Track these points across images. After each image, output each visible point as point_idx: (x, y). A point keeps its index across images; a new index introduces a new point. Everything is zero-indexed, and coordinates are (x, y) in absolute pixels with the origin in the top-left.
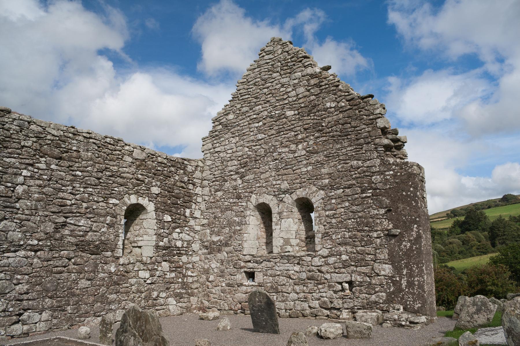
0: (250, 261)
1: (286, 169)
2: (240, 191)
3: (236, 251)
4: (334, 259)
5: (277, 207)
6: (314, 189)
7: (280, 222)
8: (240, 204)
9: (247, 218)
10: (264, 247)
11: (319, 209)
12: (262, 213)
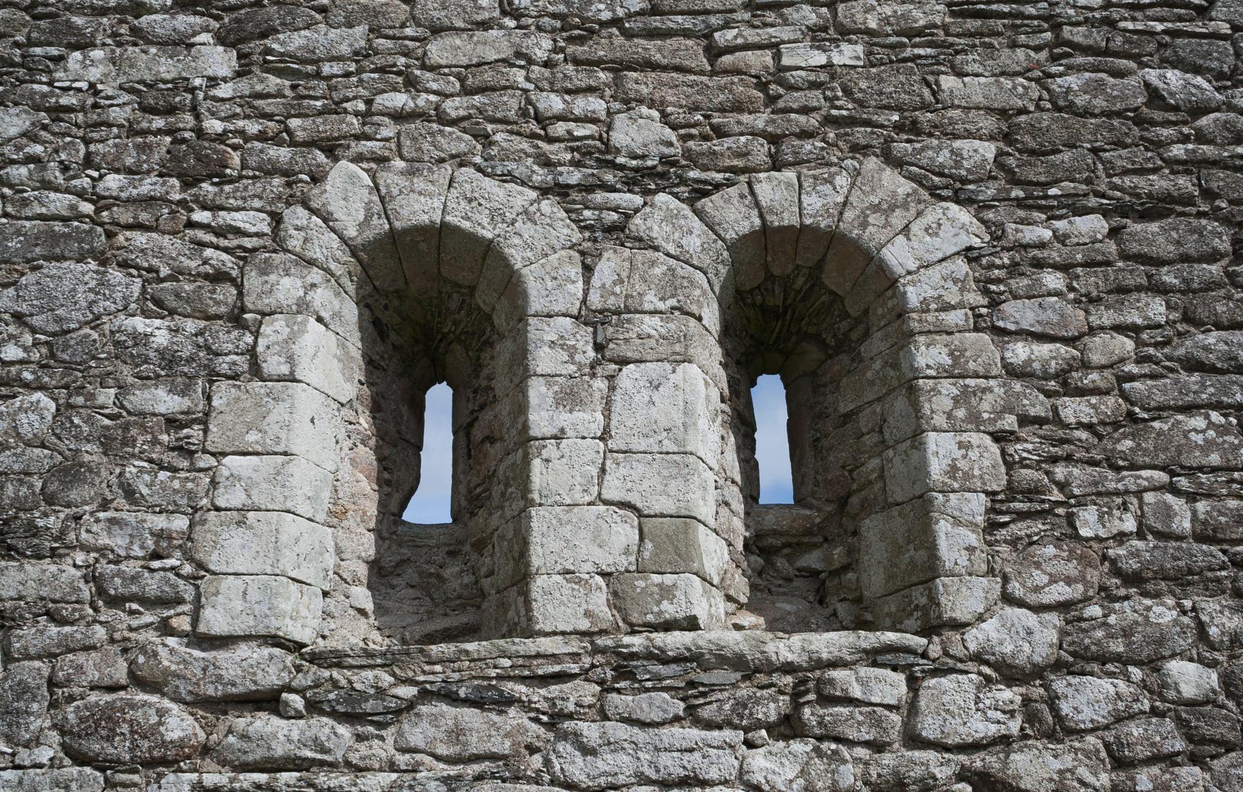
0: (269, 701)
1: (652, 34)
2: (214, 126)
3: (116, 602)
4: (1106, 686)
5: (575, 271)
6: (895, 183)
7: (600, 384)
8: (201, 216)
9: (274, 330)
10: (363, 596)
11: (955, 318)
12: (376, 323)
